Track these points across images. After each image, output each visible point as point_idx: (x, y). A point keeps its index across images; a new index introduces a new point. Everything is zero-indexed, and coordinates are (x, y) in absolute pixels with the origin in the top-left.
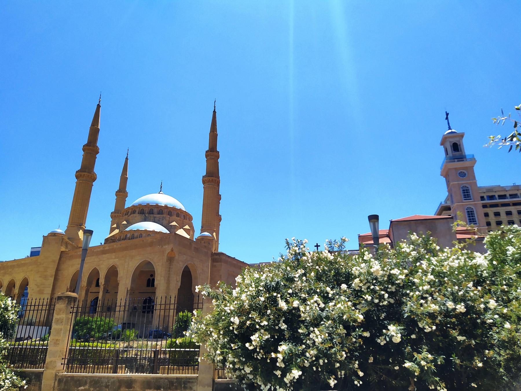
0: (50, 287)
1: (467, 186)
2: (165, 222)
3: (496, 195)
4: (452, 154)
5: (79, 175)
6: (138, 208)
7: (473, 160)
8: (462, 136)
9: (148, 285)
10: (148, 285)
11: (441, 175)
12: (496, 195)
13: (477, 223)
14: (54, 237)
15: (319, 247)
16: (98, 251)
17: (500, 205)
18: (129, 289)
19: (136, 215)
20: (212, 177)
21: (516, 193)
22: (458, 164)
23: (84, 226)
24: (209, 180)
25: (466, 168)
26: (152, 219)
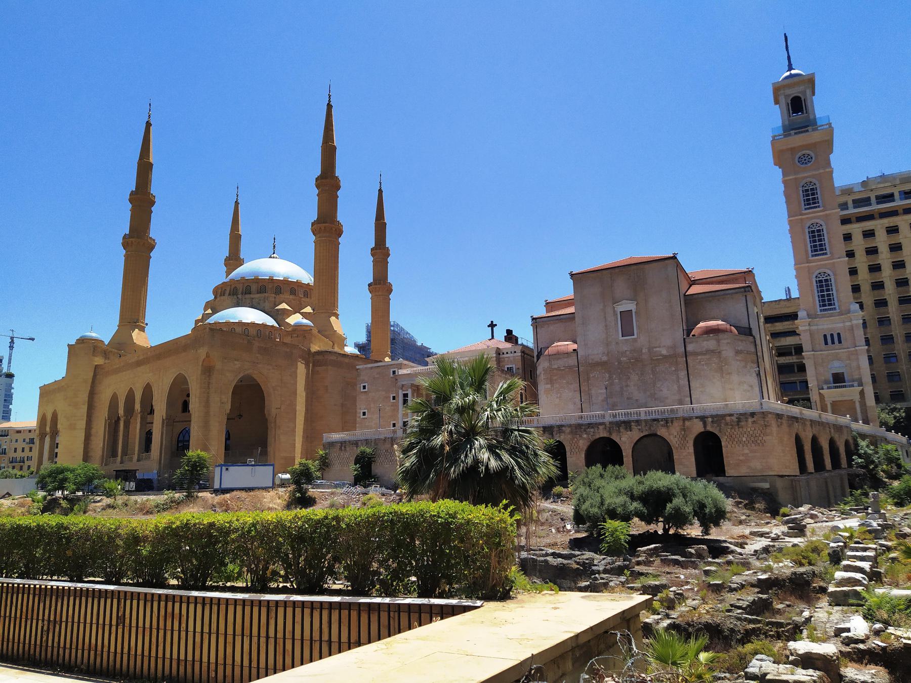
1: (814, 181)
2: (267, 306)
4: (789, 120)
6: (228, 285)
7: (830, 130)
8: (810, 82)
13: (828, 253)
14: (82, 345)
15: (495, 329)
17: (877, 216)
19: (226, 297)
22: (798, 140)
23: (143, 323)
24: (320, 228)
25: (813, 146)
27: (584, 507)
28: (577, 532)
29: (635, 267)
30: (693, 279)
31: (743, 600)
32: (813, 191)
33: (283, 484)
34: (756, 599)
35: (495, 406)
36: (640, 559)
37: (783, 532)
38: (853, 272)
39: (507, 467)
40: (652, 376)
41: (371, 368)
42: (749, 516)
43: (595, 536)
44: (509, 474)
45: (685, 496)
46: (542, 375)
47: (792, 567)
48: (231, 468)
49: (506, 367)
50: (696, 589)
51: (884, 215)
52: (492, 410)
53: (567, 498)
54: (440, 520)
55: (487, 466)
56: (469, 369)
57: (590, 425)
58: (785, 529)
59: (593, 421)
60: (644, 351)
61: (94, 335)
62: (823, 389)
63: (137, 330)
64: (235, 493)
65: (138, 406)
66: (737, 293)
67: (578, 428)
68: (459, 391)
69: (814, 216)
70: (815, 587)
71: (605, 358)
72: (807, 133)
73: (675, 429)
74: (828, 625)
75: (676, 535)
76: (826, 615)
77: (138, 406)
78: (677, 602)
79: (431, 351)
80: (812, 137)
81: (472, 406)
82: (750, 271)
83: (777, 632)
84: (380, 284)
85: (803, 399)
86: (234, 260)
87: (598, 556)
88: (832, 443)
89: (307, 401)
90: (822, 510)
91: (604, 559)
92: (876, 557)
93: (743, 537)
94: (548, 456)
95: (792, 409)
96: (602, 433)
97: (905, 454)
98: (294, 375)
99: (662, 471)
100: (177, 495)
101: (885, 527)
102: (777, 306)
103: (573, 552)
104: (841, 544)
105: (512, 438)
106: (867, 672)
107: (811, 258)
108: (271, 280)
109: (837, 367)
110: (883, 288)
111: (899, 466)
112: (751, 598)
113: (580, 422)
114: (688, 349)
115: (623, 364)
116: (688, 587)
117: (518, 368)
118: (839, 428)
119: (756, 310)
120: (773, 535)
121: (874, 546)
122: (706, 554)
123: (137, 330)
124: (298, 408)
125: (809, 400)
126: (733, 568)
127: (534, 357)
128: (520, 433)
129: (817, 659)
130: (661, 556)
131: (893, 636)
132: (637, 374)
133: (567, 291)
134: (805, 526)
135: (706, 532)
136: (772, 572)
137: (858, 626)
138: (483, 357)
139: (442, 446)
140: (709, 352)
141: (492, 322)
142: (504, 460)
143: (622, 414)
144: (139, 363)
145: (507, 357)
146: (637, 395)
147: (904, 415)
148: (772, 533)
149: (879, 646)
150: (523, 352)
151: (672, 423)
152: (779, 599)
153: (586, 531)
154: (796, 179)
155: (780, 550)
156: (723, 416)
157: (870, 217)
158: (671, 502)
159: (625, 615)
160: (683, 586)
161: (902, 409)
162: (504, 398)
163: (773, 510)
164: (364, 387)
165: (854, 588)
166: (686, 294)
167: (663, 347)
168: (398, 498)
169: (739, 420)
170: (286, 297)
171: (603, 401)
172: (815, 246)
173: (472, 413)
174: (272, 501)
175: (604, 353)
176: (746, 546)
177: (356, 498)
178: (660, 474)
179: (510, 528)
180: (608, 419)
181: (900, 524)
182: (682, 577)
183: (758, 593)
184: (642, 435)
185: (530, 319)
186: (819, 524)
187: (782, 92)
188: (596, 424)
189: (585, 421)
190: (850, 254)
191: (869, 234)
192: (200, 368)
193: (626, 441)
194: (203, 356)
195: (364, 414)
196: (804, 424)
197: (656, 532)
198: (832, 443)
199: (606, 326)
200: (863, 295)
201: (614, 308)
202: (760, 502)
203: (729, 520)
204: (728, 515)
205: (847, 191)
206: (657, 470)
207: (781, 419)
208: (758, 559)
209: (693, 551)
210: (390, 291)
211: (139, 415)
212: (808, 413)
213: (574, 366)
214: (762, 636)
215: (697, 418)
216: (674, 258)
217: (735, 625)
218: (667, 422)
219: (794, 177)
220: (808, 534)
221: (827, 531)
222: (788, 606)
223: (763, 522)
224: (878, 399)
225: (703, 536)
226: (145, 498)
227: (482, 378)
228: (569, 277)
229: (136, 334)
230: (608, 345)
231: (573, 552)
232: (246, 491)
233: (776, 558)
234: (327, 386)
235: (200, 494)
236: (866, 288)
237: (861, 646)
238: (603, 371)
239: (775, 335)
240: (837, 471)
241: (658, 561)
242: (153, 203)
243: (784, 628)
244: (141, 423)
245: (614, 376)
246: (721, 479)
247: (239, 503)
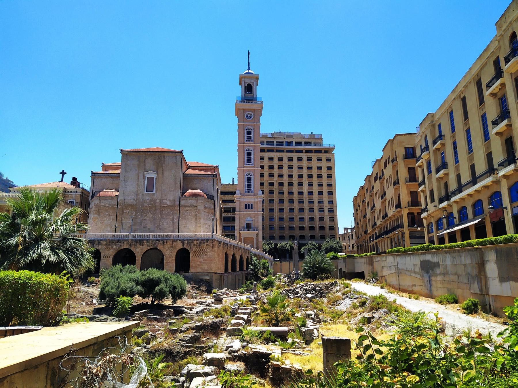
1: (252, 128)
3: (294, 141)
12: (294, 141)
17: (275, 151)
21: (311, 141)
22: (247, 106)
25: (253, 111)
27: (107, 289)
28: (99, 304)
29: (159, 153)
30: (189, 166)
31: (186, 337)
34: (193, 336)
35: (59, 223)
36: (135, 318)
37: (212, 302)
38: (262, 176)
39: (62, 261)
40: (159, 216)
42: (197, 294)
43: (111, 306)
44: (62, 266)
45: (166, 282)
46: (93, 208)
47: (213, 319)
49: (69, 200)
50: (163, 333)
51: (307, 152)
52: (56, 226)
53: (97, 284)
54: (20, 281)
55: (48, 260)
56: (44, 198)
57: (119, 241)
58: (213, 300)
60: (157, 201)
62: (241, 231)
66: (209, 177)
67: (111, 242)
68: (35, 211)
69: (249, 145)
70: (222, 329)
71: (134, 203)
73: (168, 246)
74: (224, 345)
75: (158, 304)
76: (224, 340)
78: (152, 340)
79: (14, 183)
80: (254, 106)
81: (43, 222)
82: (217, 167)
83: (200, 352)
85: (232, 235)
87: (110, 317)
88: (241, 257)
90: (232, 291)
91: (113, 319)
92: (250, 313)
93: (192, 304)
94: (90, 256)
95: (226, 239)
96: (126, 246)
97: (271, 265)
99: (157, 269)
101: (257, 299)
102: (227, 187)
103: (95, 316)
104: (237, 307)
105: (68, 244)
106: (236, 365)
109: (249, 220)
111: (268, 271)
112: (190, 336)
113: (113, 238)
114: (181, 203)
115: (144, 207)
116: (159, 332)
117: (77, 203)
118: (245, 250)
119: (217, 187)
120: (207, 303)
121: (250, 308)
122: (172, 314)
125: (234, 235)
126: (185, 320)
127: (89, 197)
128: (74, 241)
129: (215, 361)
130: (148, 316)
131: (250, 348)
132: (152, 214)
133: (117, 159)
134: (222, 299)
135: (174, 302)
136: (203, 322)
137: (236, 344)
138: (55, 191)
139: (17, 245)
140: (192, 206)
141: (63, 171)
142: (61, 256)
143: (139, 235)
145: (70, 195)
146: (149, 225)
147: (273, 246)
148: (206, 302)
149: (243, 353)
150: (82, 193)
151: (166, 243)
152: (204, 335)
153: (105, 304)
155: (209, 310)
156: (193, 241)
158: (159, 286)
159: (125, 329)
160: (156, 332)
161: (273, 243)
162: (67, 218)
163: (209, 291)
165: (239, 327)
166: (185, 173)
167: (169, 200)
169: (201, 243)
171: (129, 227)
172: (248, 160)
173: (42, 226)
175: (134, 200)
176: (193, 309)
178: (155, 270)
179: (65, 287)
180: (130, 238)
181: (263, 298)
182: (157, 327)
183: (194, 332)
184: (149, 248)
186: (229, 298)
188: (123, 240)
189: (116, 238)
190: (262, 167)
193: (139, 251)
196: (230, 248)
197: (147, 303)
198: (241, 257)
200: (284, 188)
201: (144, 174)
202: (203, 287)
203: (187, 296)
204: (186, 294)
205: (265, 136)
206: (154, 268)
207: (220, 244)
208: (198, 315)
209: (165, 313)
212: (233, 242)
213: (115, 205)
214: (192, 355)
215: (180, 240)
216: (181, 152)
217: (180, 349)
218: (164, 242)
219: (243, 124)
220: (223, 303)
221: (232, 301)
222: (208, 339)
223: (203, 297)
224: (264, 238)
225: (172, 304)
227: (53, 204)
228: (120, 151)
231: (95, 316)
233: (206, 314)
236: (266, 184)
237: (236, 354)
238: (132, 210)
239: (224, 201)
240: (241, 272)
241: (145, 319)
243: (204, 349)
245: (138, 213)
246: (187, 274)
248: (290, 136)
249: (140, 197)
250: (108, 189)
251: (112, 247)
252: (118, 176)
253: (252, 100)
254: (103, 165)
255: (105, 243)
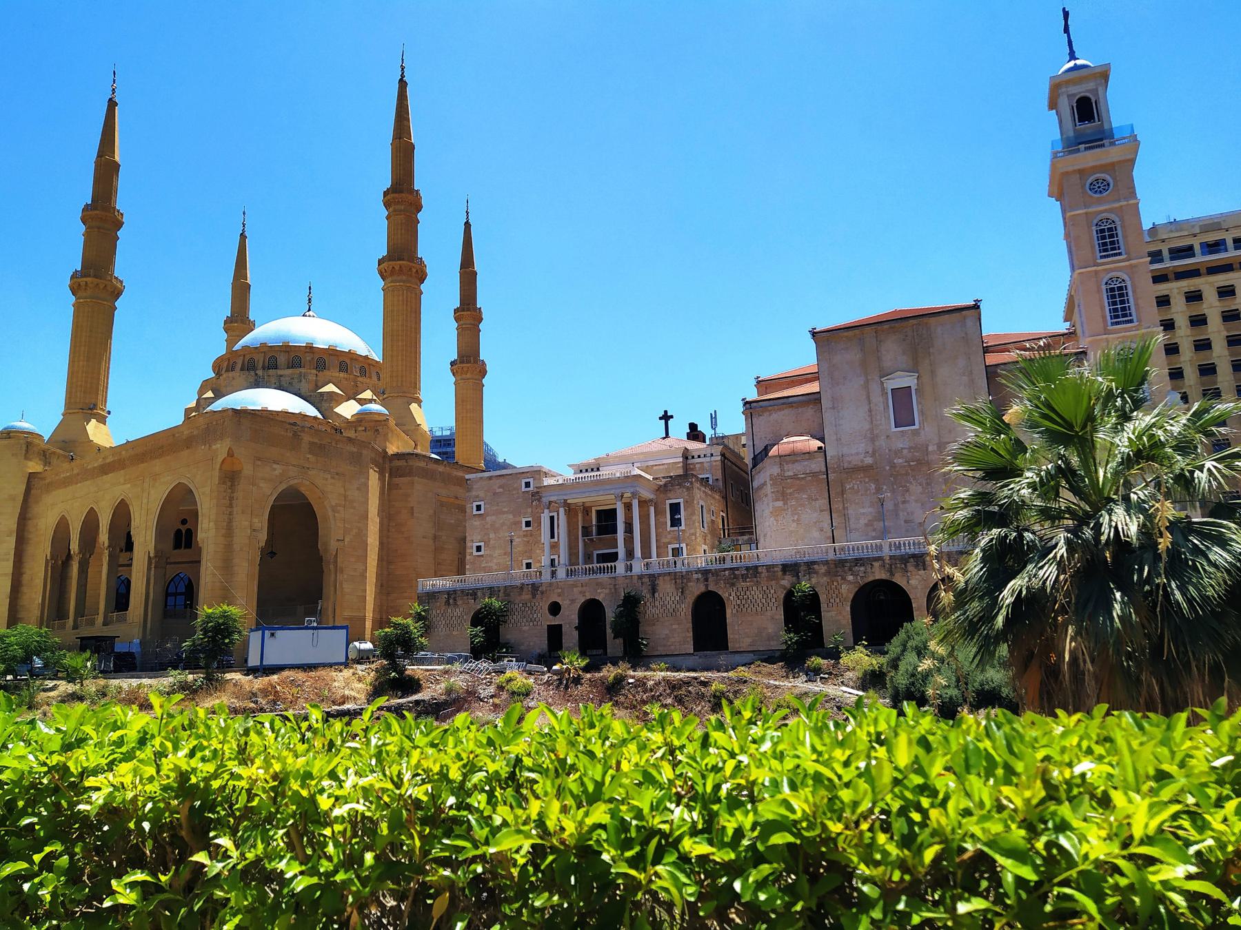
0: (8, 560)
1: (1113, 217)
2: (304, 387)
4: (1075, 130)
5: (77, 285)
7: (1134, 142)
9: (177, 546)
10: (177, 546)
11: (1050, 195)
15: (670, 422)
16: (94, 468)
17: (1171, 276)
18: (152, 555)
19: (236, 373)
20: (399, 259)
22: (1088, 158)
25: (1110, 167)
26: (273, 380)
32: (1112, 232)
33: (363, 658)
41: (490, 478)
48: (279, 633)
51: (1214, 270)
57: (858, 561)
59: (865, 554)
60: (930, 448)
61: (25, 425)
63: (93, 421)
64: (286, 673)
65: (104, 537)
67: (839, 566)
69: (1114, 267)
71: (869, 460)
72: (1103, 149)
77: (104, 537)
84: (468, 362)
86: (239, 321)
89: (381, 531)
96: (879, 574)
98: (364, 488)
100: (190, 677)
107: (1110, 328)
108: (310, 348)
110: (1215, 372)
123: (93, 421)
124: (370, 541)
133: (805, 357)
141: (666, 412)
143: (909, 543)
144: (106, 469)
154: (1086, 213)
157: (1193, 273)
164: (479, 508)
168: (556, 677)
170: (334, 374)
171: (866, 525)
172: (1116, 310)
174: (347, 684)
177: (485, 678)
180: (886, 552)
185: (741, 404)
187: (1064, 90)
191: (1194, 297)
192: (216, 473)
194: (222, 455)
195: (479, 549)
199: (870, 411)
200: (1220, 379)
201: (882, 383)
210: (483, 373)
211: (107, 552)
226: (134, 682)
228: (809, 335)
229: (92, 428)
230: (873, 439)
232: (305, 671)
234: (412, 508)
235: (228, 676)
242: (119, 225)
244: (109, 565)
247: (295, 690)
248: (1213, 225)
249: (882, 442)
250: (788, 435)
251: (844, 579)
252: (815, 399)
253: (1101, 140)
254: (758, 382)
255: (823, 569)
